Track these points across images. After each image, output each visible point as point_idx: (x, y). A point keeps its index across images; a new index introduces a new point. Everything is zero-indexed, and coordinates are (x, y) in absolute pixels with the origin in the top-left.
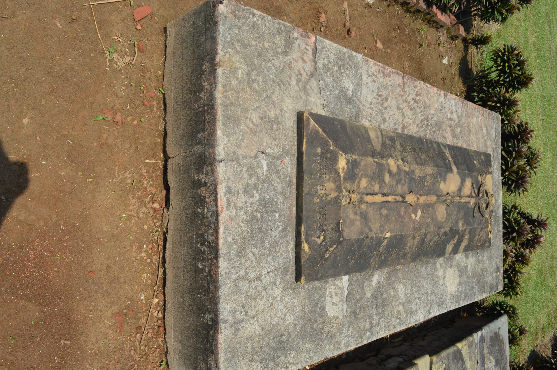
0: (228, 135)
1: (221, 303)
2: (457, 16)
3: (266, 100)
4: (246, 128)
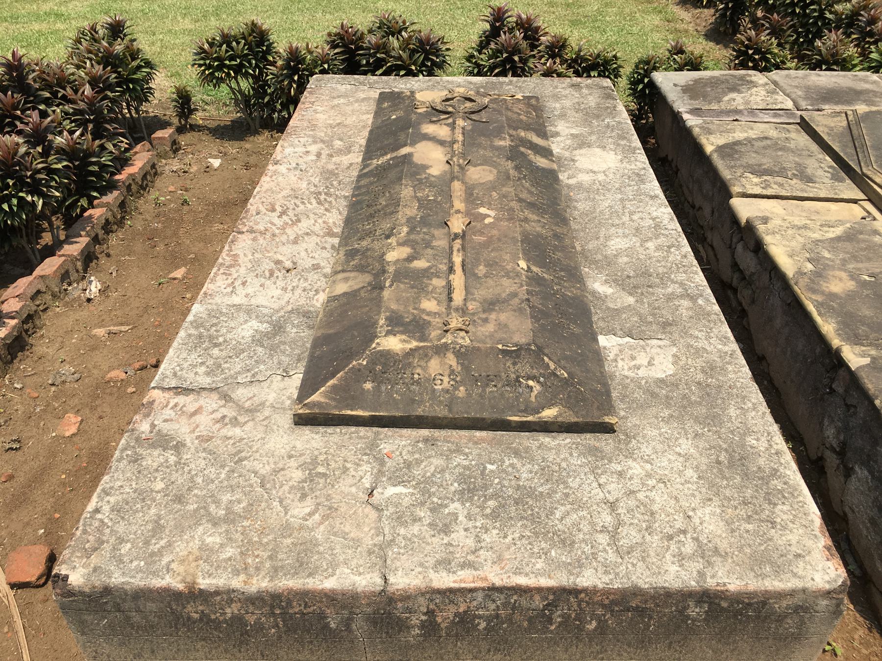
0: (334, 566)
1: (667, 585)
2: (137, 141)
3: (268, 486)
4: (322, 528)
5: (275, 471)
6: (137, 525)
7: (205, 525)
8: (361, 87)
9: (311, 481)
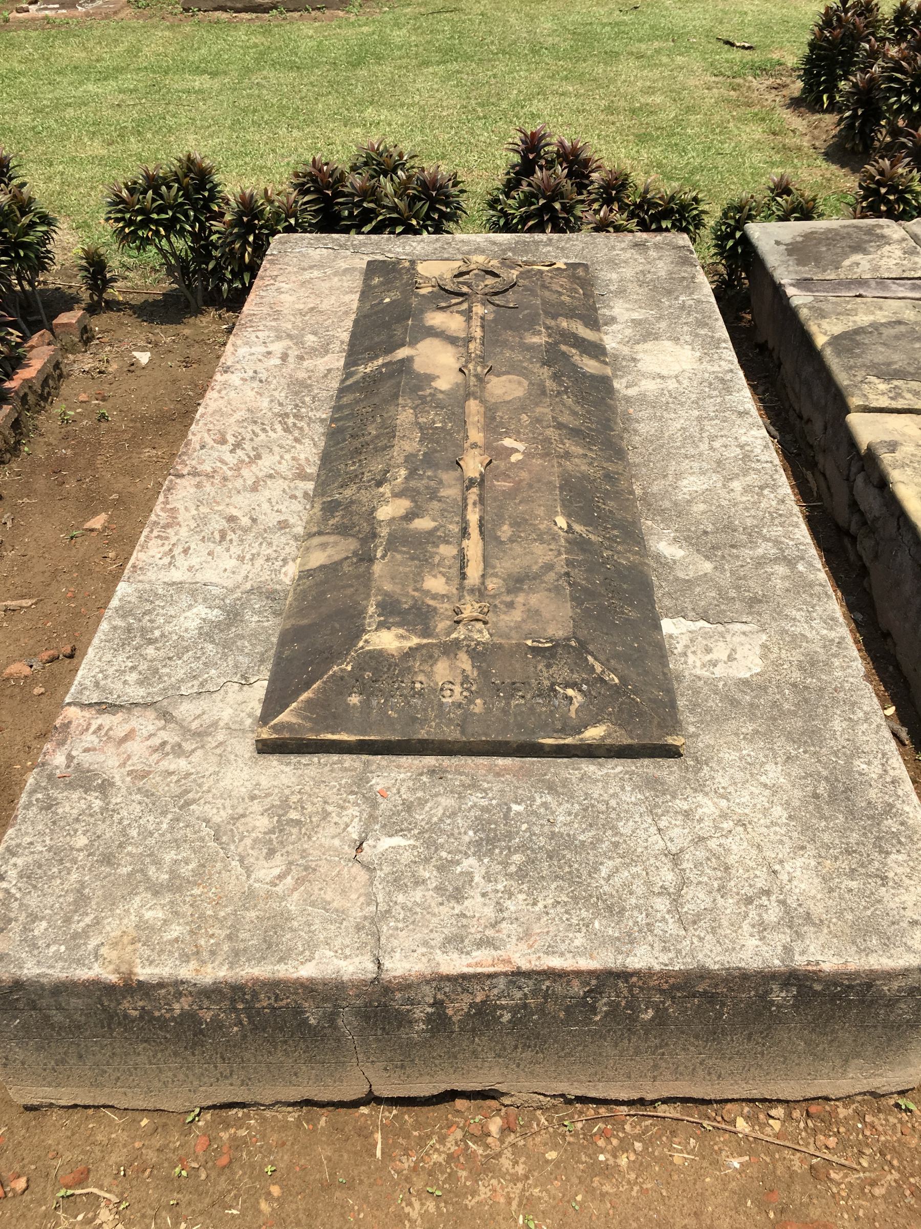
0: (311, 946)
1: (742, 965)
2: (35, 327)
3: (224, 839)
4: (296, 895)
5: (233, 818)
6: (52, 897)
7: (143, 895)
8: (343, 252)
9: (281, 831)
